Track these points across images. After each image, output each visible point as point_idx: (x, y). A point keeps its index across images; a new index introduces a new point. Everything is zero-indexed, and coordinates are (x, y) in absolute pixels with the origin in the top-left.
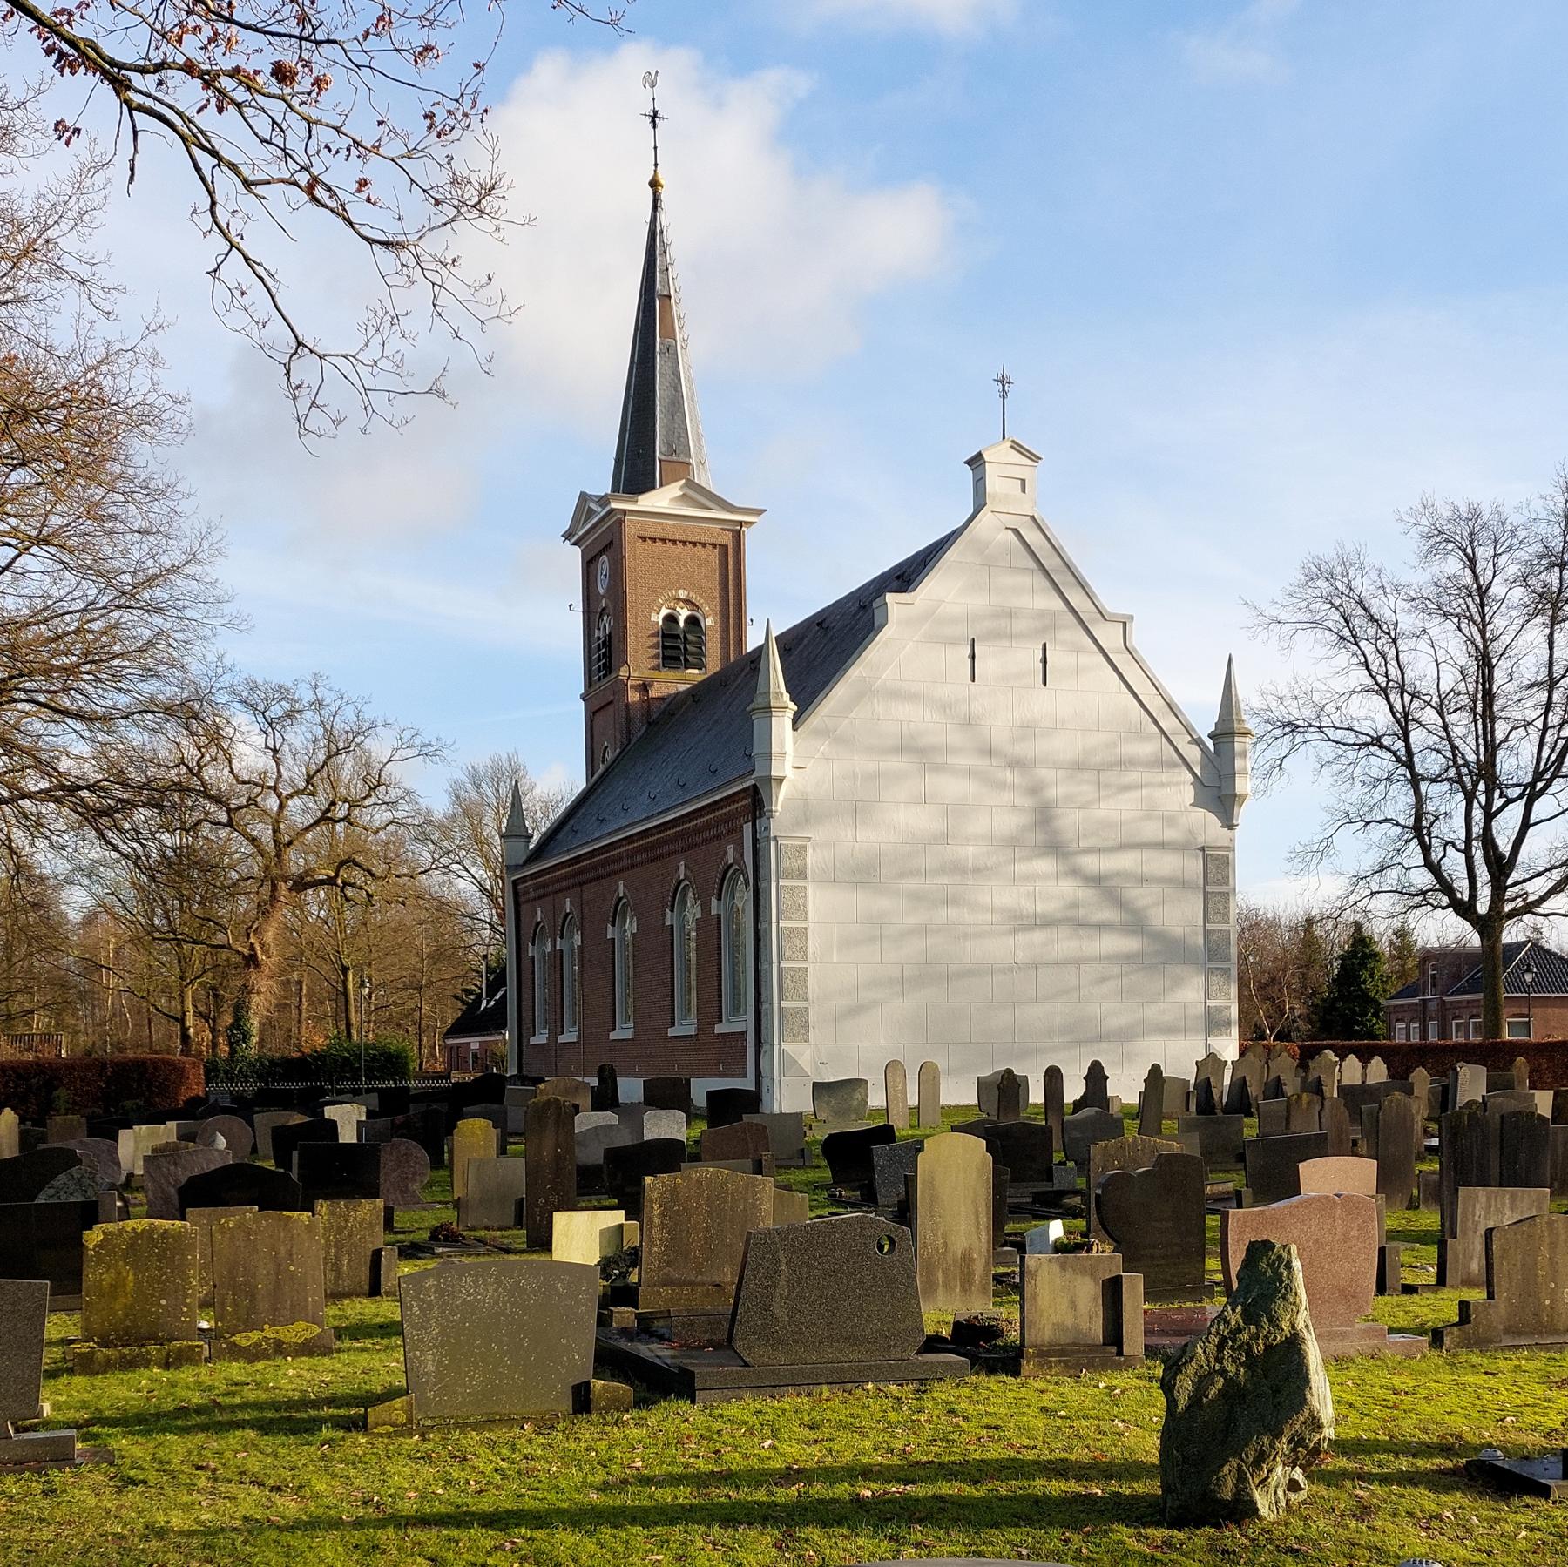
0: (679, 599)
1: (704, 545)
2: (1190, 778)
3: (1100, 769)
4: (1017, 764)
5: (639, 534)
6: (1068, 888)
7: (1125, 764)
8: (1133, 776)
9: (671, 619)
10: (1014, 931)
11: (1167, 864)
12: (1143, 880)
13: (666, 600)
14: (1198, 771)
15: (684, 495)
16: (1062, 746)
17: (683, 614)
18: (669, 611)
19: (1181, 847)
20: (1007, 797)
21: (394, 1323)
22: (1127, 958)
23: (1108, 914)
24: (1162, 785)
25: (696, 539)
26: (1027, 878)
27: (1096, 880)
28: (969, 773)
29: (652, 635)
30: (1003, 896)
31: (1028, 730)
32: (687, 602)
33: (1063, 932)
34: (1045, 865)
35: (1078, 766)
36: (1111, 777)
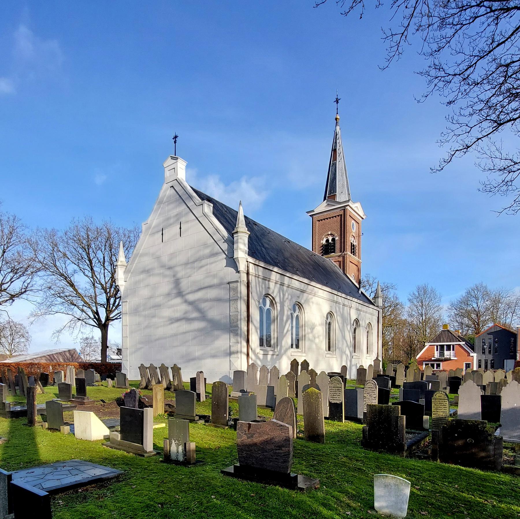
0: (329, 235)
1: (327, 219)
2: (225, 256)
3: (194, 262)
4: (170, 268)
5: (317, 220)
6: (184, 307)
7: (200, 259)
8: (204, 262)
9: (327, 241)
10: (172, 323)
11: (212, 293)
12: (206, 301)
13: (325, 236)
14: (226, 253)
15: (328, 204)
16: (181, 259)
17: (330, 238)
18: (327, 239)
19: (219, 285)
20: (167, 279)
21: (427, 429)
22: (200, 330)
23: (195, 315)
24: (212, 263)
25: (330, 217)
26: (172, 306)
27: (191, 303)
28: (159, 274)
29: (321, 247)
30: (167, 313)
31: (173, 256)
32: (331, 234)
33: (183, 322)
34: (178, 300)
35: (186, 264)
36: (196, 264)
